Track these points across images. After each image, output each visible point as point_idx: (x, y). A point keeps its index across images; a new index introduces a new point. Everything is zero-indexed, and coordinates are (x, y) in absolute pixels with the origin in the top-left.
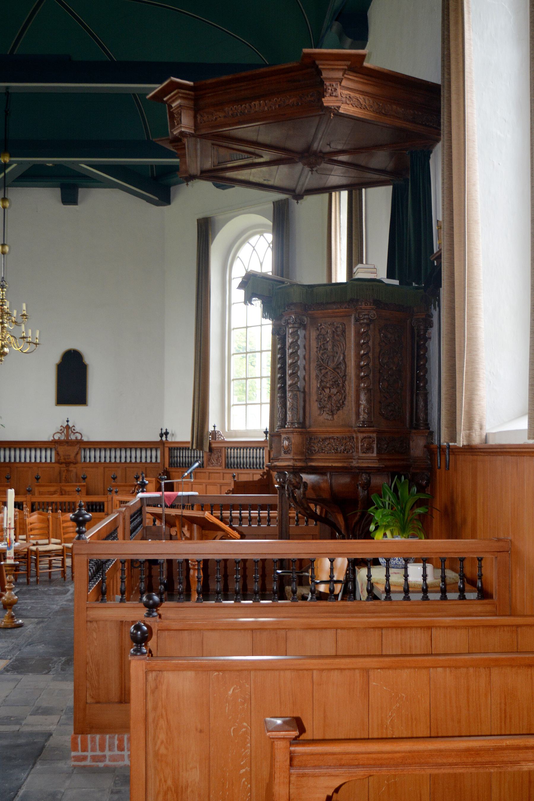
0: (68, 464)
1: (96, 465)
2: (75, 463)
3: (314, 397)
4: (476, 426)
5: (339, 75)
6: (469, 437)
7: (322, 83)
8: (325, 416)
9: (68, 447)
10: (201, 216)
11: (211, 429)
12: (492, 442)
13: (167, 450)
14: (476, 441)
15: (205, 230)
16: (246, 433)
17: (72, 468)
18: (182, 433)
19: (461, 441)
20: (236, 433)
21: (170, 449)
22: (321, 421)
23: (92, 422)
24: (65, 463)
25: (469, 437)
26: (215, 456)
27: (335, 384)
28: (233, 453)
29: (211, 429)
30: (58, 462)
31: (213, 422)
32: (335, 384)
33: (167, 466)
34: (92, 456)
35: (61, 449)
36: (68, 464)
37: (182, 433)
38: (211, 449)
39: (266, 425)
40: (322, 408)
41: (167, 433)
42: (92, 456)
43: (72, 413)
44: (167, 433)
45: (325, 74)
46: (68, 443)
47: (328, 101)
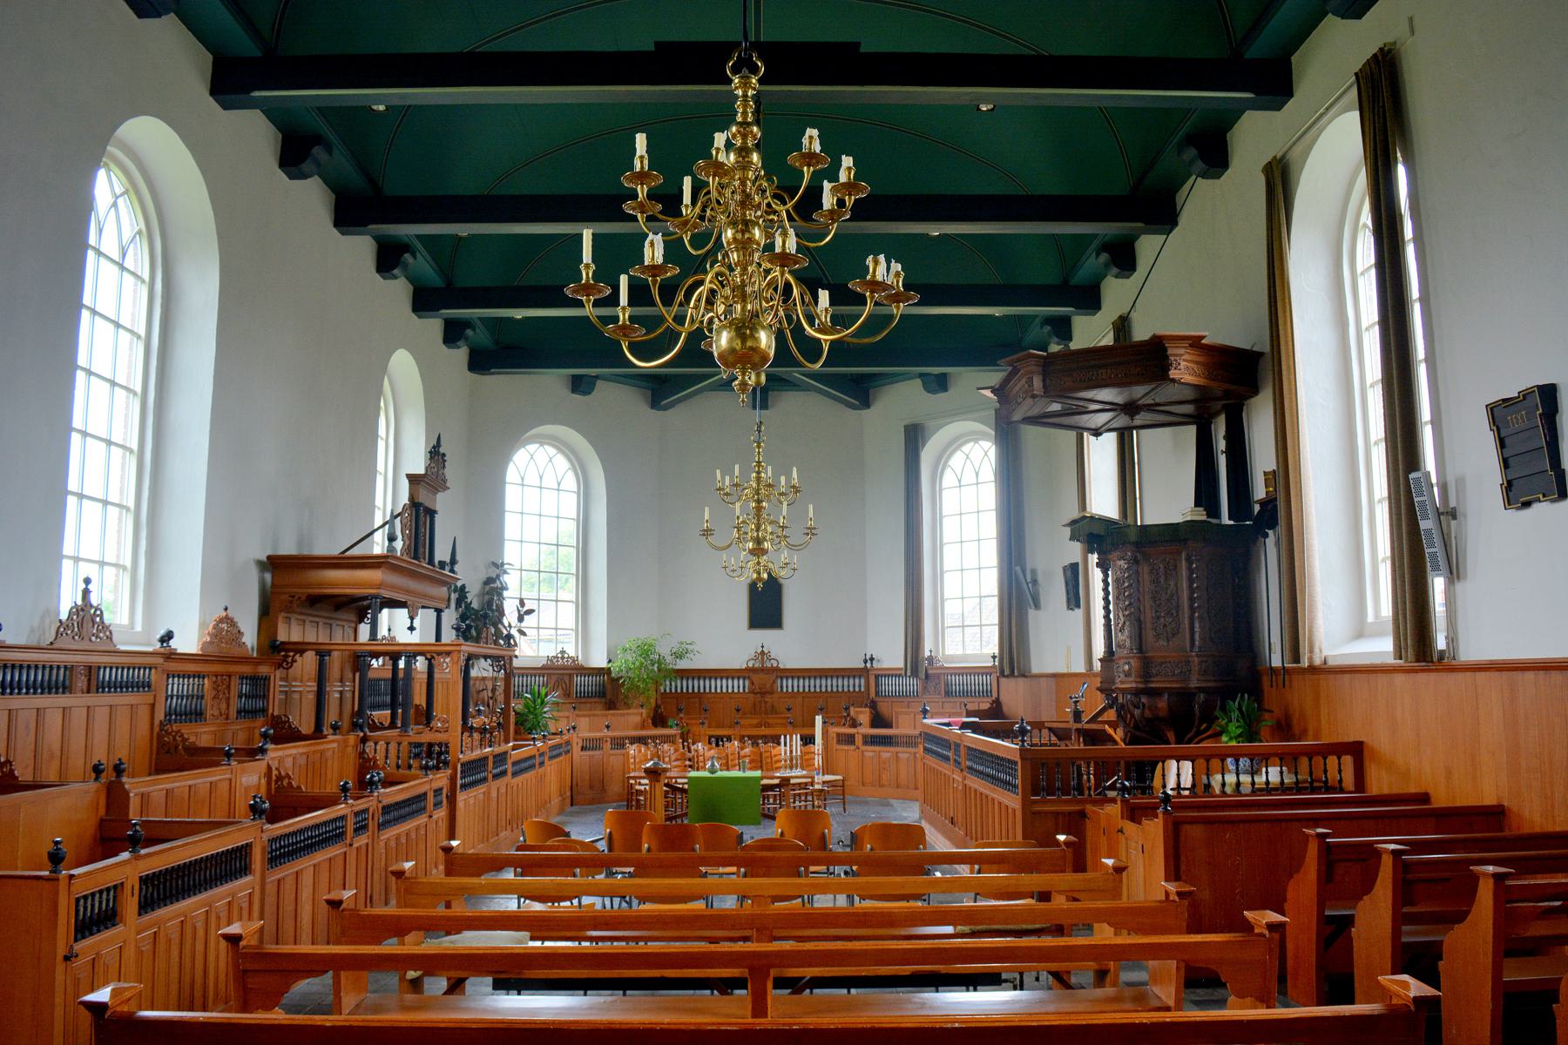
0: (763, 694)
1: (793, 695)
2: (772, 693)
3: (1149, 626)
4: (1317, 650)
5: (1182, 351)
6: (1310, 659)
7: (1167, 357)
8: (1163, 643)
9: (763, 675)
10: (907, 422)
11: (927, 654)
12: (1331, 663)
13: (872, 679)
14: (1317, 662)
15: (914, 437)
16: (965, 657)
17: (768, 698)
18: (891, 656)
19: (1305, 663)
20: (952, 658)
21: (877, 677)
22: (1158, 647)
23: (789, 647)
24: (761, 692)
25: (1310, 659)
26: (931, 685)
27: (1169, 613)
28: (955, 679)
29: (927, 654)
30: (752, 692)
31: (928, 648)
32: (1169, 613)
33: (873, 694)
34: (789, 685)
35: (755, 677)
36: (763, 694)
37: (891, 656)
38: (927, 676)
39: (993, 648)
40: (1158, 636)
41: (872, 659)
42: (789, 685)
43: (766, 638)
44: (872, 659)
45: (1170, 352)
46: (763, 670)
47: (1173, 374)
